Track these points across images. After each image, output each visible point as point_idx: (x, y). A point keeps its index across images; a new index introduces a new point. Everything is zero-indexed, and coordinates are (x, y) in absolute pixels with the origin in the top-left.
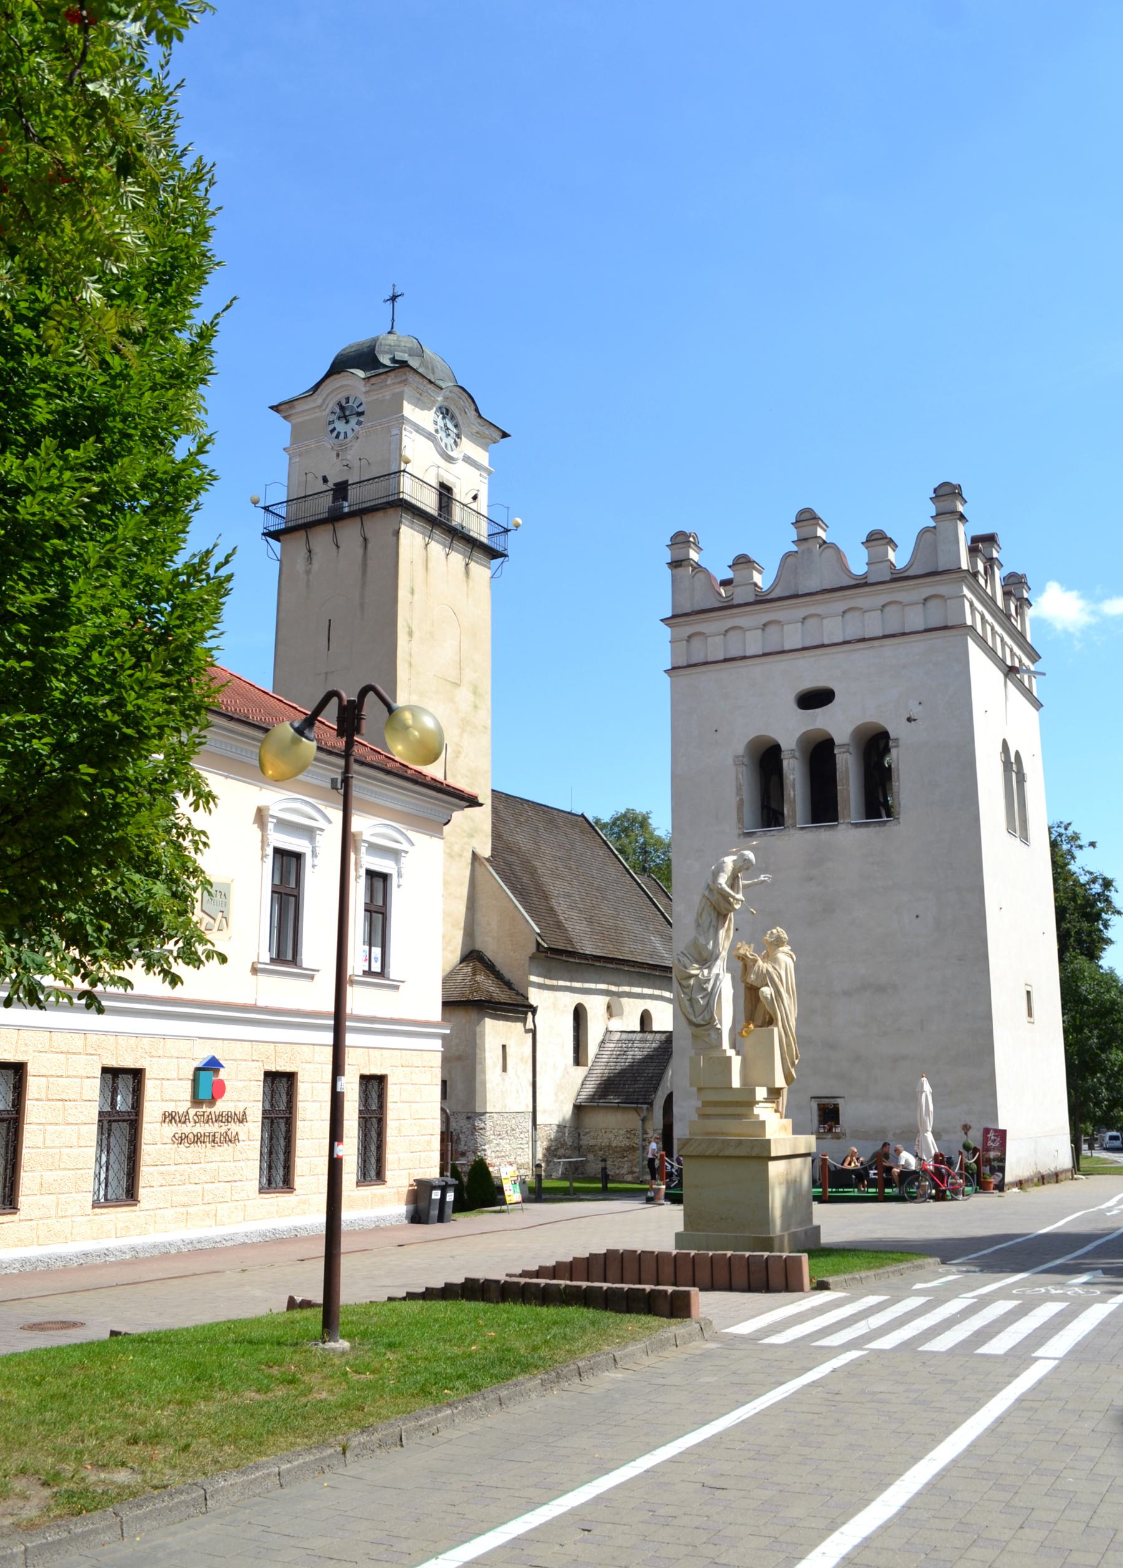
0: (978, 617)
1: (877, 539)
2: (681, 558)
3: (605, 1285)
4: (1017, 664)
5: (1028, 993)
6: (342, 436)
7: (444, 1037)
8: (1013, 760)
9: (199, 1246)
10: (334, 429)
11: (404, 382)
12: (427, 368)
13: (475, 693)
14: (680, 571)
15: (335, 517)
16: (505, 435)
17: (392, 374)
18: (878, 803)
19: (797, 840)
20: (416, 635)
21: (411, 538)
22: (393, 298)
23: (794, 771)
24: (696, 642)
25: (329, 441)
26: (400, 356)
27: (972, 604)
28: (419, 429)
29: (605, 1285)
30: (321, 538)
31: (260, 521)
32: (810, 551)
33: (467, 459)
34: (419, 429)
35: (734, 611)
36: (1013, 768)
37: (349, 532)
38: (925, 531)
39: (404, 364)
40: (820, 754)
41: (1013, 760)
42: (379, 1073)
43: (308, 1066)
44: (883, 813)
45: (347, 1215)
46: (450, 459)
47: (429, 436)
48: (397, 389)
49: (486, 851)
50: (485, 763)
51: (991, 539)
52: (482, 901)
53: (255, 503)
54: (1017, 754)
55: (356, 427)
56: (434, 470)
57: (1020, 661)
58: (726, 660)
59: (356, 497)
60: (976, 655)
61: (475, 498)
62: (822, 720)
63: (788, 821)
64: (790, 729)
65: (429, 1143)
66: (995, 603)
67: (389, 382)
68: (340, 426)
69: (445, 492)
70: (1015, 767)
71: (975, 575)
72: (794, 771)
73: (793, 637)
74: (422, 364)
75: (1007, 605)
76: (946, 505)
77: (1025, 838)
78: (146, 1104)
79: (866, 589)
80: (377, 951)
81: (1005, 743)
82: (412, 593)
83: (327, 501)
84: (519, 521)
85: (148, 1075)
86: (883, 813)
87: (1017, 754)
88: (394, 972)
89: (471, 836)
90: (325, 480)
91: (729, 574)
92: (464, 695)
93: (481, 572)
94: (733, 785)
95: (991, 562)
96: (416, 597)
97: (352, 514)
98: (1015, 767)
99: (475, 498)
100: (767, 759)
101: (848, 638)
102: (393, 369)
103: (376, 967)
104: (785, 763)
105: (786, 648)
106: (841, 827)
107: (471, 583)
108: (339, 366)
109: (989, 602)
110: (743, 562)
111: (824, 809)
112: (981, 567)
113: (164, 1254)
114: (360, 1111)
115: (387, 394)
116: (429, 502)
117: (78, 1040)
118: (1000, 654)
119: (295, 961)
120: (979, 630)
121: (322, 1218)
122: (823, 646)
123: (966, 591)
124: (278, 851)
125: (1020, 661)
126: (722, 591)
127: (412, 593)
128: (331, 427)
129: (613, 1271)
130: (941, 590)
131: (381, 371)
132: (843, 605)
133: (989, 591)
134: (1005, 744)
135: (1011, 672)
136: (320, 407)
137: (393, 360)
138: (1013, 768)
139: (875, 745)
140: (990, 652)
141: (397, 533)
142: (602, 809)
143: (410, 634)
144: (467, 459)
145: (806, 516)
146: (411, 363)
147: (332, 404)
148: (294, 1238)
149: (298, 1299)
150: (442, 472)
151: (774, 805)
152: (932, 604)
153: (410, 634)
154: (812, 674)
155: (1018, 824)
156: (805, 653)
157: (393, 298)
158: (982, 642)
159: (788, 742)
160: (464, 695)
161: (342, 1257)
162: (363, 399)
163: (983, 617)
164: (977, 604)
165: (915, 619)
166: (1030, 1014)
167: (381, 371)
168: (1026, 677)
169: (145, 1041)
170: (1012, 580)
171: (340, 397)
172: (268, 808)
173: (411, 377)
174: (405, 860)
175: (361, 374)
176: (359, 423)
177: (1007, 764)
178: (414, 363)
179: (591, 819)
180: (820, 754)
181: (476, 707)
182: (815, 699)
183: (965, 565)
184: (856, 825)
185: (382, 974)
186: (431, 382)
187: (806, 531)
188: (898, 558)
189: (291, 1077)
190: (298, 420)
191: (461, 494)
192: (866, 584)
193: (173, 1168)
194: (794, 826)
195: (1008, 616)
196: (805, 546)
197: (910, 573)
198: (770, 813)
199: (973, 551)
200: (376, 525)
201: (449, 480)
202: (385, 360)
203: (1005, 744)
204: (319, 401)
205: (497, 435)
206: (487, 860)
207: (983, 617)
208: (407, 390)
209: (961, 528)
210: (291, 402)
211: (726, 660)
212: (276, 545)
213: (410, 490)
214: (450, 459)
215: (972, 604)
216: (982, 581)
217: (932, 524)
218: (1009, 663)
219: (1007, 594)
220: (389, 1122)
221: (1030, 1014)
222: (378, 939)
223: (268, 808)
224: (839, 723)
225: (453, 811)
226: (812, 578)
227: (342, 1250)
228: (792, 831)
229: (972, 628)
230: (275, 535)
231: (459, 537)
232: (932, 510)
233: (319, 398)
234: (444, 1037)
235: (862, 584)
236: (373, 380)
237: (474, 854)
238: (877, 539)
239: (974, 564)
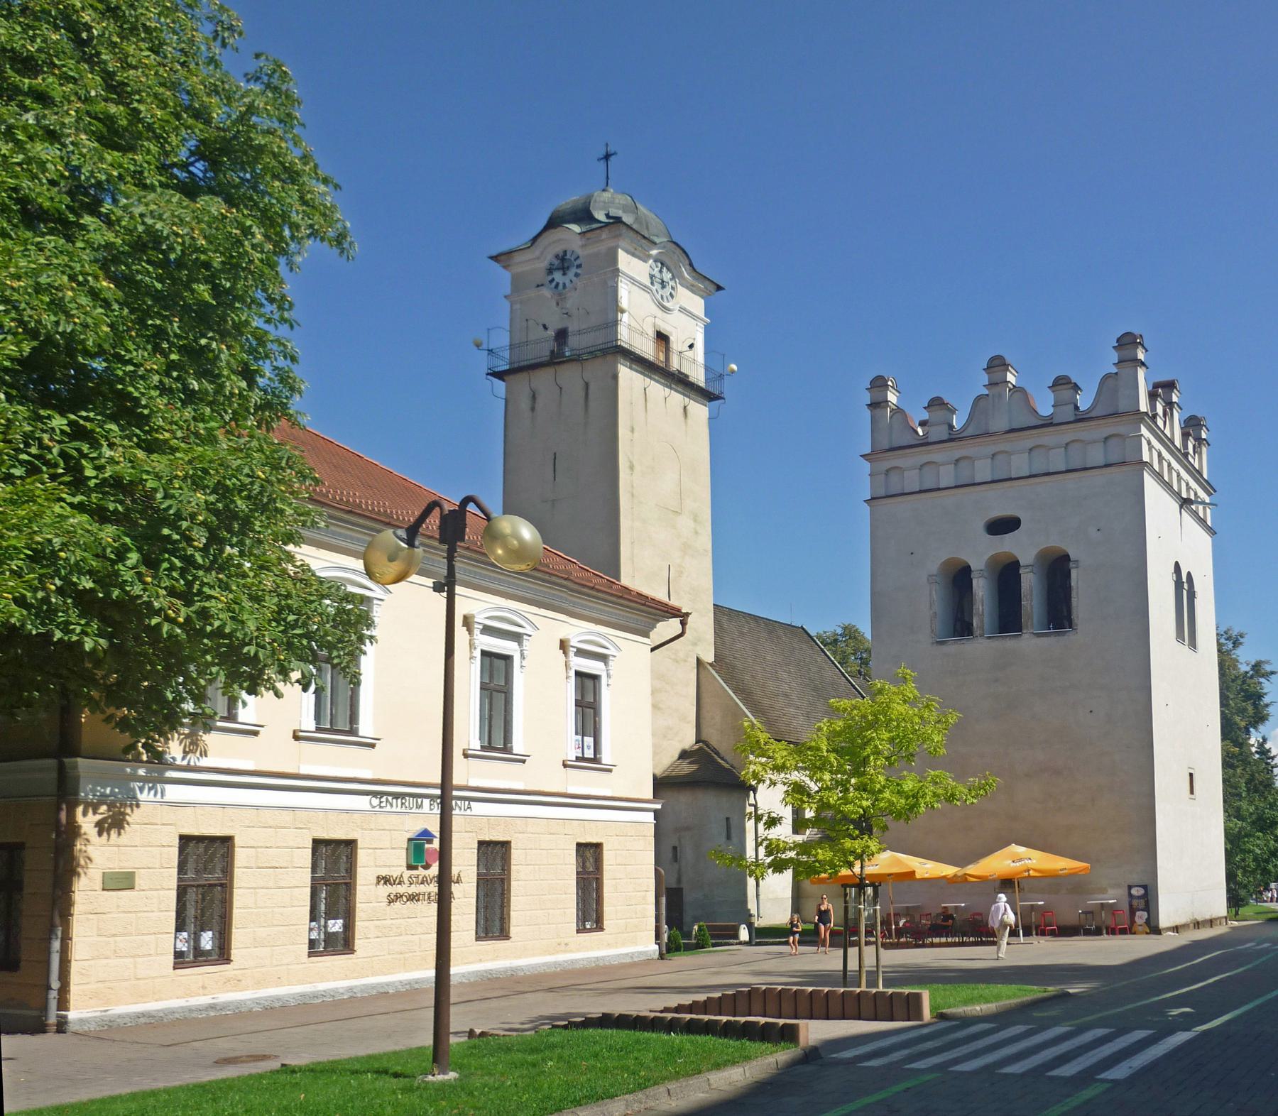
0: (1175, 475)
1: (1062, 383)
2: (880, 399)
3: (762, 1020)
4: (1192, 497)
5: (1191, 775)
6: (561, 287)
7: (656, 812)
8: (1184, 579)
9: (417, 986)
10: (553, 280)
11: (618, 236)
12: (641, 223)
13: (695, 521)
14: (878, 412)
15: (556, 360)
16: (719, 288)
17: (606, 230)
18: (1059, 614)
19: (982, 648)
20: (637, 468)
21: (628, 377)
22: (607, 157)
23: (981, 588)
24: (894, 478)
25: (546, 292)
26: (613, 212)
27: (1149, 443)
28: (633, 281)
29: (762, 1020)
30: (543, 379)
31: (482, 363)
32: (1001, 396)
33: (683, 310)
34: (633, 281)
35: (930, 447)
36: (1184, 586)
37: (570, 376)
38: (1107, 377)
39: (618, 220)
40: (1007, 575)
41: (1184, 579)
42: (594, 841)
43: (520, 836)
44: (1066, 624)
45: (457, 969)
46: (666, 309)
47: (644, 287)
48: (611, 243)
49: (709, 657)
50: (707, 582)
51: (1170, 386)
52: (706, 700)
53: (478, 346)
54: (1189, 574)
55: (574, 279)
56: (650, 320)
57: (1196, 494)
58: (921, 492)
59: (574, 342)
60: (1151, 486)
61: (691, 346)
62: (1008, 544)
63: (977, 632)
64: (980, 553)
65: (644, 898)
66: (1173, 443)
67: (604, 236)
68: (558, 276)
69: (662, 338)
70: (1186, 586)
71: (1154, 417)
72: (981, 588)
73: (983, 471)
74: (637, 219)
75: (1186, 447)
76: (1127, 353)
77: (1193, 644)
78: (359, 870)
79: (1051, 429)
80: (589, 741)
81: (1177, 564)
82: (632, 430)
83: (550, 345)
84: (734, 367)
85: (360, 844)
86: (1066, 624)
87: (1189, 574)
88: (606, 758)
89: (695, 644)
90: (545, 327)
91: (925, 416)
92: (685, 523)
93: (700, 411)
94: (929, 602)
95: (1169, 404)
96: (636, 434)
97: (571, 360)
98: (1186, 586)
99: (691, 346)
100: (960, 578)
101: (1034, 473)
102: (607, 224)
103: (589, 754)
104: (974, 582)
105: (977, 481)
106: (1025, 636)
107: (689, 421)
108: (555, 222)
109: (1167, 442)
110: (936, 403)
111: (1009, 621)
112: (1160, 409)
113: (382, 995)
114: (578, 873)
115: (602, 248)
116: (647, 348)
117: (287, 817)
118: (1166, 478)
119: (506, 748)
120: (1156, 467)
121: (432, 973)
122: (1011, 479)
123: (1144, 431)
124: (485, 654)
125: (1196, 494)
126: (920, 431)
127: (632, 430)
128: (550, 278)
129: (757, 1006)
130: (1121, 429)
131: (594, 226)
132: (1029, 443)
133: (1167, 432)
134: (1177, 565)
135: (1185, 503)
136: (538, 258)
137: (608, 216)
138: (1184, 586)
139: (1057, 569)
140: (1168, 486)
141: (615, 377)
142: (821, 625)
143: (632, 468)
144: (683, 310)
145: (997, 362)
146: (625, 219)
147: (549, 258)
148: (410, 991)
149: (478, 1031)
150: (659, 322)
151: (967, 619)
152: (1112, 442)
153: (632, 468)
154: (1000, 504)
155: (1186, 630)
156: (994, 485)
157: (607, 157)
158: (1158, 476)
159: (977, 563)
160: (685, 523)
161: (453, 1010)
162: (579, 252)
163: (1160, 455)
164: (1155, 442)
165: (1096, 455)
166: (1192, 792)
167: (594, 226)
168: (1201, 507)
169: (356, 816)
170: (1192, 422)
171: (558, 249)
172: (473, 616)
173: (624, 230)
174: (612, 663)
175: (576, 228)
176: (577, 275)
177: (1178, 584)
178: (627, 219)
179: (813, 634)
180: (1007, 575)
181: (696, 533)
182: (1003, 526)
183: (1144, 406)
184: (1038, 635)
185: (596, 760)
186: (644, 237)
187: (997, 376)
188: (1084, 401)
189: (598, 847)
190: (518, 269)
191: (677, 344)
192: (1051, 425)
193: (389, 922)
194: (982, 636)
195: (1186, 455)
196: (996, 390)
197: (1093, 414)
198: (961, 626)
199: (1153, 396)
200: (593, 370)
201: (666, 328)
202: (600, 216)
203: (1177, 565)
204: (537, 253)
205: (712, 288)
206: (711, 665)
207: (1160, 455)
208: (622, 243)
209: (1141, 373)
210: (509, 253)
211: (921, 492)
212: (500, 386)
213: (626, 336)
214: (666, 309)
215: (1149, 443)
216: (1160, 422)
217: (1114, 370)
218: (1184, 495)
219: (1185, 436)
220: (605, 881)
221: (1192, 792)
222: (590, 728)
223: (473, 616)
224: (1023, 547)
225: (658, 621)
226: (1001, 420)
227: (452, 1000)
228: (980, 640)
229: (1149, 465)
230: (500, 375)
231: (680, 381)
232: (1115, 357)
233: (536, 251)
234: (656, 812)
235: (1048, 423)
236: (588, 235)
237: (698, 660)
238: (1062, 383)
239: (1153, 407)
